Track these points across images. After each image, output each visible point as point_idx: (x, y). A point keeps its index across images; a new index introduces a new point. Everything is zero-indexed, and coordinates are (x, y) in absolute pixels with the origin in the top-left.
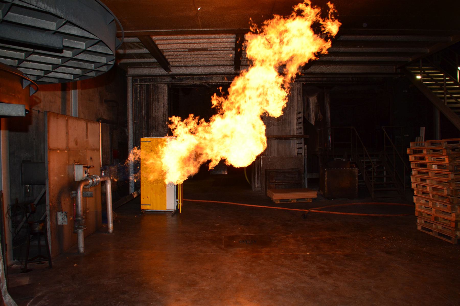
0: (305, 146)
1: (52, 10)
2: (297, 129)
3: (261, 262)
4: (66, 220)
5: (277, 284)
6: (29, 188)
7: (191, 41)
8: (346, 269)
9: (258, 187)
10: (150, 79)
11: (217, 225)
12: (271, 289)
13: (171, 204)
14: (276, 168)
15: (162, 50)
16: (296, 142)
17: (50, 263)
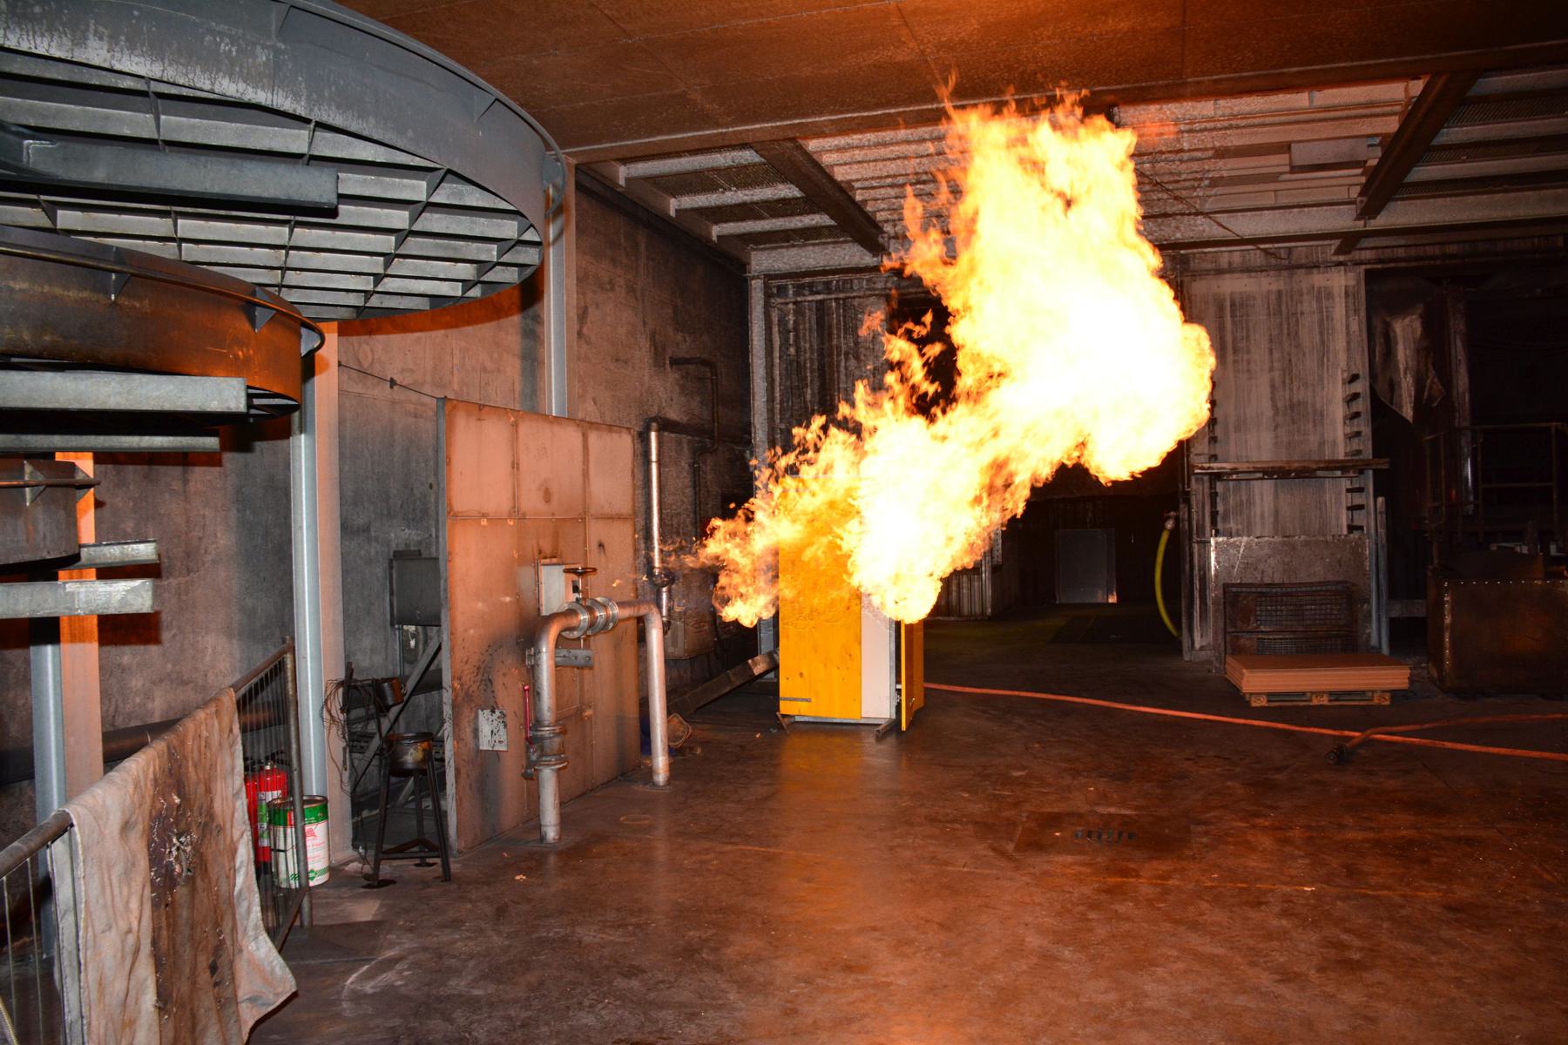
0: (1380, 500)
1: (261, 97)
2: (1350, 437)
3: (1121, 908)
4: (504, 738)
5: (1148, 988)
6: (414, 636)
7: (904, 149)
8: (1434, 959)
9: (1202, 648)
10: (828, 284)
11: (1016, 774)
12: (1122, 1003)
13: (877, 696)
14: (1267, 580)
15: (849, 182)
16: (1345, 484)
17: (446, 865)
